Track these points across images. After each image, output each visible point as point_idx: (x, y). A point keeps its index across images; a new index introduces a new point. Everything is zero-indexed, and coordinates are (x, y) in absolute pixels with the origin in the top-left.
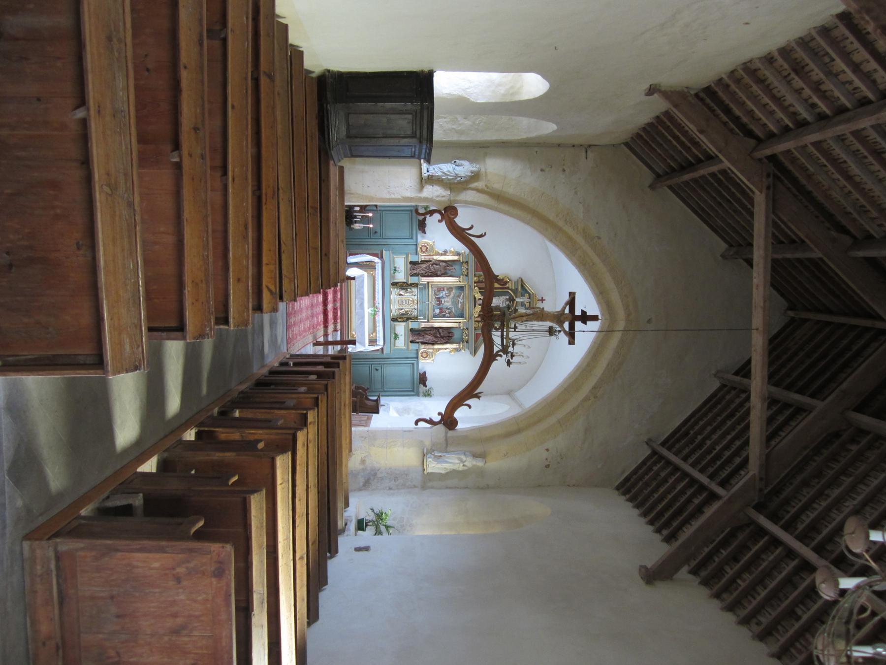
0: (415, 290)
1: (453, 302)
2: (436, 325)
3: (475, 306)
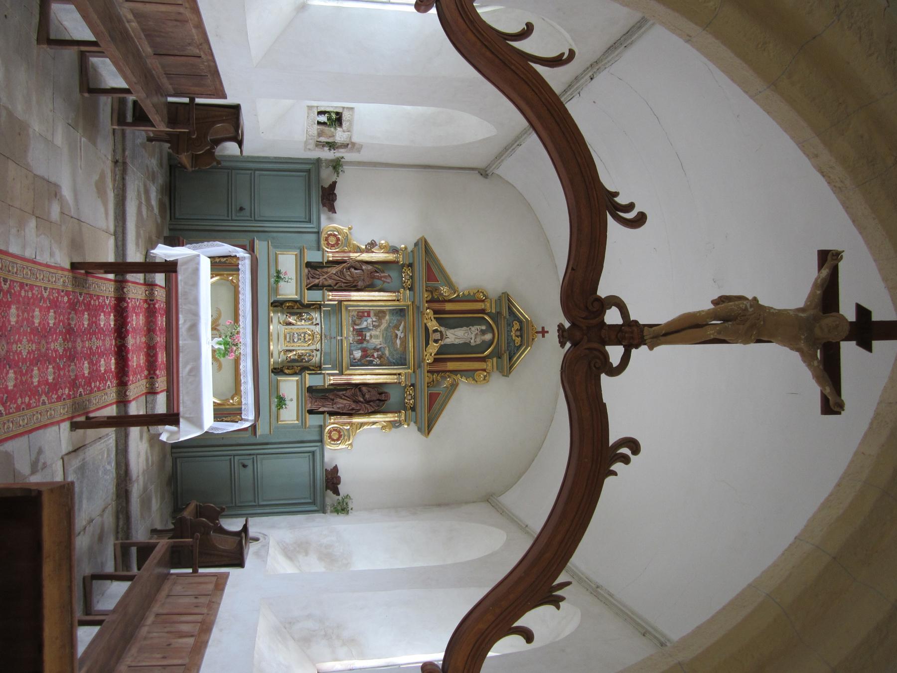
2: (357, 379)
3: (427, 344)
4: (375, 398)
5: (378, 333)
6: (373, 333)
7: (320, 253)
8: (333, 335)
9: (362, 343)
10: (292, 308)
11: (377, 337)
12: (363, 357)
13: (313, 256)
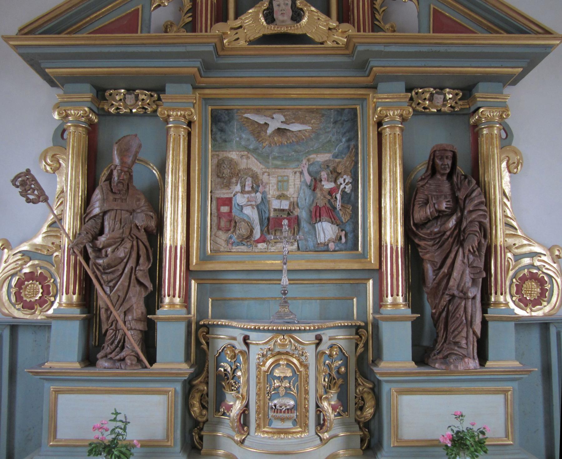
0: (227, 336)
1: (286, 161)
2: (394, 234)
3: (302, 39)
4: (446, 187)
5: (273, 180)
6: (272, 191)
7: (54, 324)
8: (273, 291)
9: (297, 219)
10: (204, 397)
11: (283, 182)
12: (334, 220)
13: (68, 342)
